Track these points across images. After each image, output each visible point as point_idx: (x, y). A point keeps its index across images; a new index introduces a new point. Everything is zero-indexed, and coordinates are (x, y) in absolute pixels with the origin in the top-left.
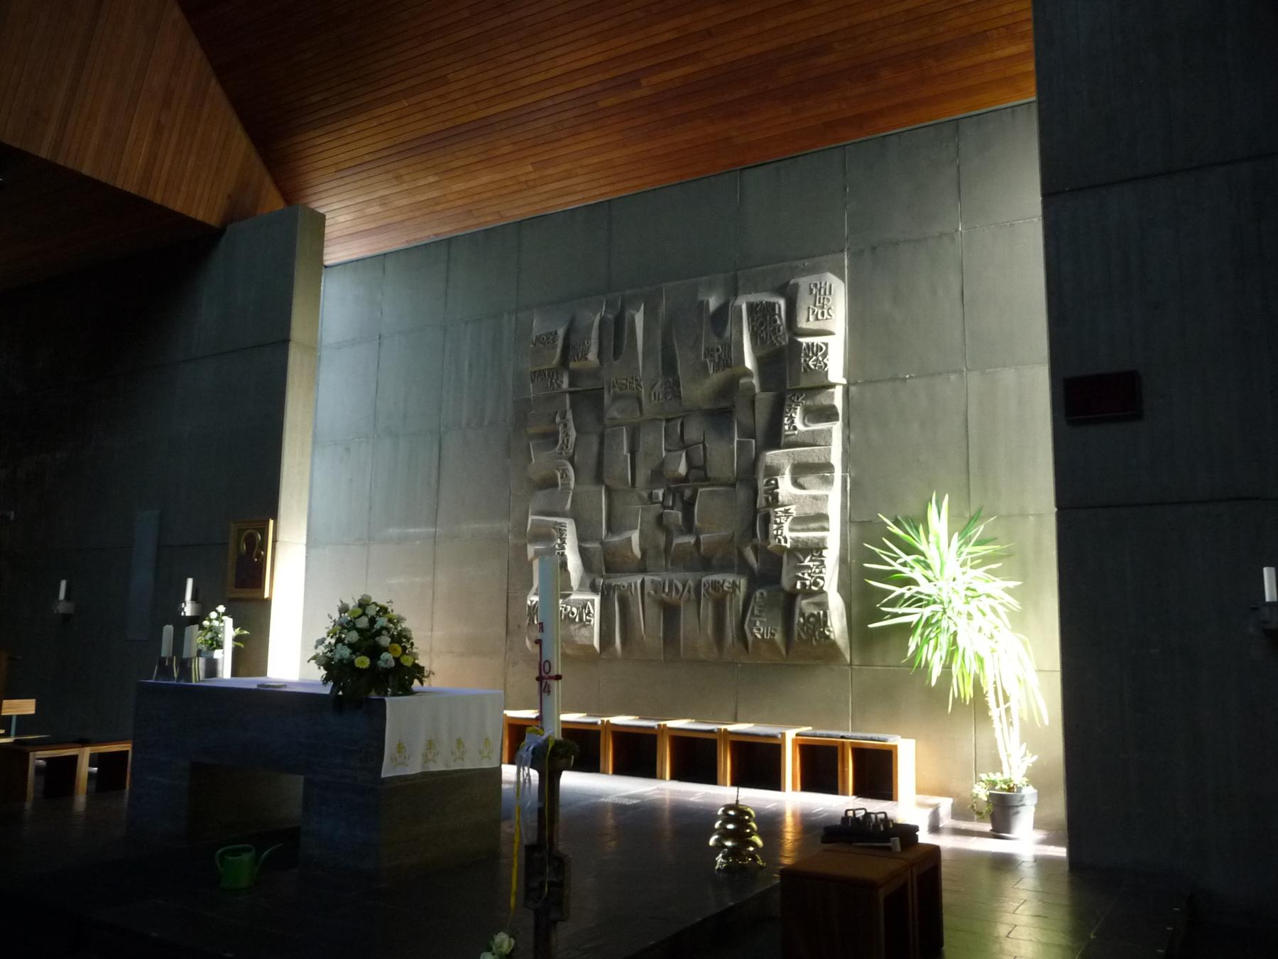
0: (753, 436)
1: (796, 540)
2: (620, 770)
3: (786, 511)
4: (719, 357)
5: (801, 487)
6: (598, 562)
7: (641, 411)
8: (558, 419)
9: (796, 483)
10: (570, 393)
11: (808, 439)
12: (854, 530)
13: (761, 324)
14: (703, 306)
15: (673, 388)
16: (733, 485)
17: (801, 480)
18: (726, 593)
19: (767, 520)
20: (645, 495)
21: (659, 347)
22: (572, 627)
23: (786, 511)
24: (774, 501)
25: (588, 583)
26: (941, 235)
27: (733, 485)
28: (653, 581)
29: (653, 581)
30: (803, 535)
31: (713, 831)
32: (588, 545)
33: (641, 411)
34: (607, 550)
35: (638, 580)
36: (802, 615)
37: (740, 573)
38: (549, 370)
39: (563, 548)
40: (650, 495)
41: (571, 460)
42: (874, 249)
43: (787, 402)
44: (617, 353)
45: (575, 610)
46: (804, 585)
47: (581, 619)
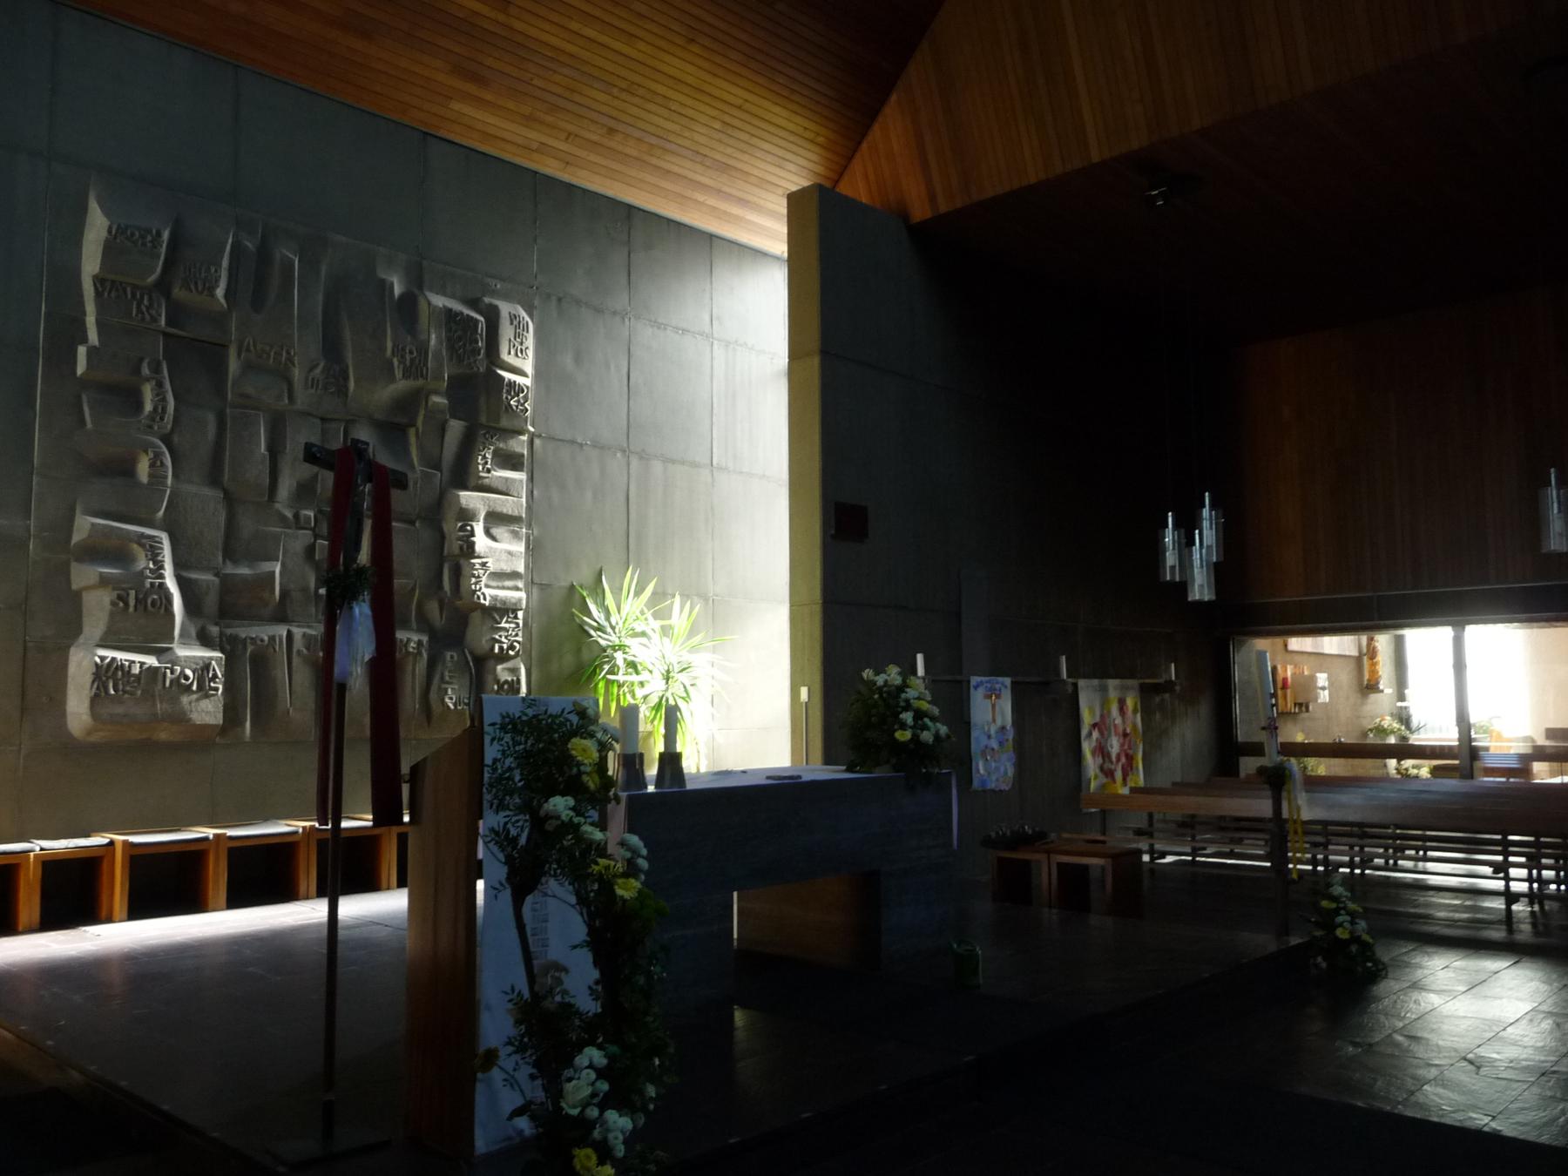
0: (437, 467)
1: (494, 598)
2: (140, 909)
3: (484, 564)
4: (412, 360)
5: (494, 539)
6: (211, 602)
7: (291, 398)
8: (146, 371)
9: (488, 533)
10: (165, 334)
11: (501, 487)
12: (535, 590)
13: (460, 339)
14: (384, 287)
15: (336, 381)
16: (412, 523)
17: (495, 531)
18: (408, 653)
19: (457, 573)
20: (289, 514)
21: (320, 318)
22: (185, 699)
23: (484, 564)
24: (469, 550)
25: (193, 632)
26: (615, 313)
27: (412, 523)
28: (304, 635)
29: (304, 635)
30: (502, 594)
31: (1363, 874)
32: (194, 575)
33: (291, 398)
34: (228, 586)
35: (282, 631)
36: (498, 682)
37: (420, 630)
38: (135, 287)
39: (162, 577)
40: (296, 516)
41: (167, 440)
42: (560, 300)
43: (481, 439)
44: (258, 302)
45: (189, 672)
46: (501, 648)
47: (200, 687)
